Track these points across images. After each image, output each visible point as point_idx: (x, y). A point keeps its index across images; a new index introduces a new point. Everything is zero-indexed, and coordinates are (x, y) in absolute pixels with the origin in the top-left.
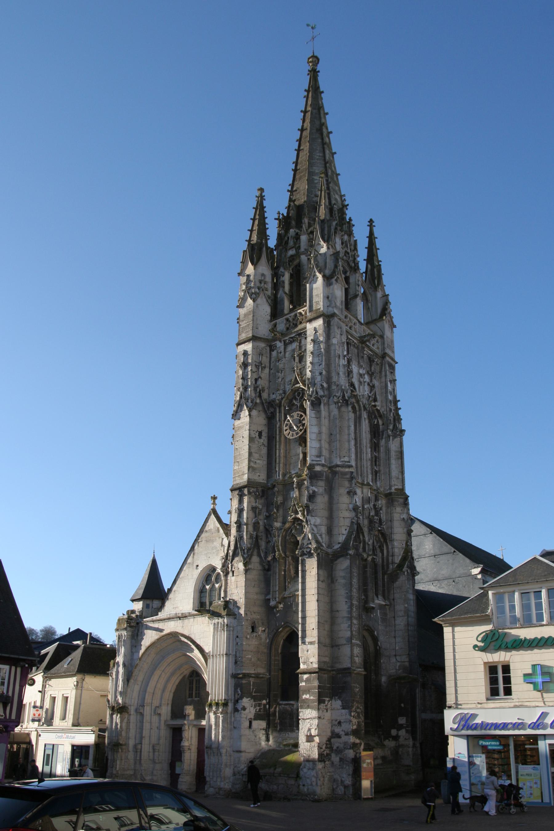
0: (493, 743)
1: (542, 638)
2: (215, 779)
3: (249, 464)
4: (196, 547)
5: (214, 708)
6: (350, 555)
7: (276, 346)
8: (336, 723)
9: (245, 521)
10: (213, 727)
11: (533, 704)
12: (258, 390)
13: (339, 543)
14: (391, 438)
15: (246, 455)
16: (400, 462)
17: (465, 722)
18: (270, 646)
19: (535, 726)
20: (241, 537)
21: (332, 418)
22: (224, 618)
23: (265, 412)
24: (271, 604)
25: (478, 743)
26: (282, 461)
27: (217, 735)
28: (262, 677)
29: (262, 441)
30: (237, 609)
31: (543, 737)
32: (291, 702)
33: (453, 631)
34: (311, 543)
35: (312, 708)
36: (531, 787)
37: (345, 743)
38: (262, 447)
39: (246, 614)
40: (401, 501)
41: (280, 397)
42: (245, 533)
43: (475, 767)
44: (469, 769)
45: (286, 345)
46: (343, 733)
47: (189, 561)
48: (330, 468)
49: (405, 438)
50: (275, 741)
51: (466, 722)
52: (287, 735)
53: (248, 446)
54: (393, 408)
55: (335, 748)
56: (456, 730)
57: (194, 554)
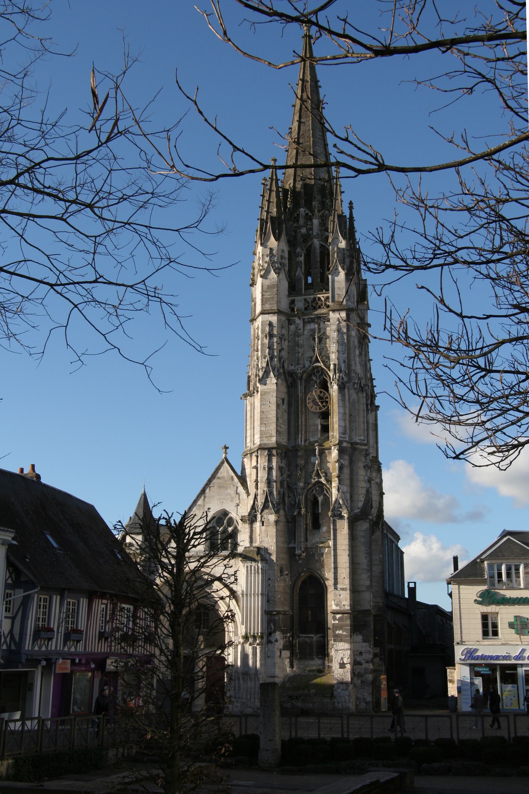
0: (485, 669)
1: (522, 598)
2: (252, 700)
3: (277, 428)
4: (207, 491)
5: (251, 640)
6: (369, 519)
7: (295, 322)
8: (358, 653)
9: (274, 478)
10: (251, 656)
11: (514, 643)
12: (282, 361)
13: (359, 508)
14: (370, 412)
15: (274, 419)
16: (375, 434)
17: (470, 654)
18: (293, 587)
19: (517, 658)
20: (271, 493)
21: (351, 401)
22: (258, 562)
23: (286, 381)
24: (296, 553)
25: (474, 669)
26: (303, 430)
27: (255, 662)
28: (288, 614)
29: (284, 407)
30: (268, 555)
31: (520, 666)
32: (311, 635)
33: (459, 588)
34: (341, 507)
35: (345, 641)
36: (511, 699)
37: (366, 669)
38: (285, 413)
39: (277, 560)
40: (376, 467)
41: (301, 371)
42: (275, 490)
43: (475, 686)
44: (471, 687)
45: (305, 323)
46: (364, 661)
47: (200, 502)
48: (352, 444)
49: (379, 412)
50: (298, 668)
51: (471, 654)
52: (307, 662)
53: (275, 412)
54: (370, 385)
55: (356, 673)
56: (463, 660)
57: (205, 497)
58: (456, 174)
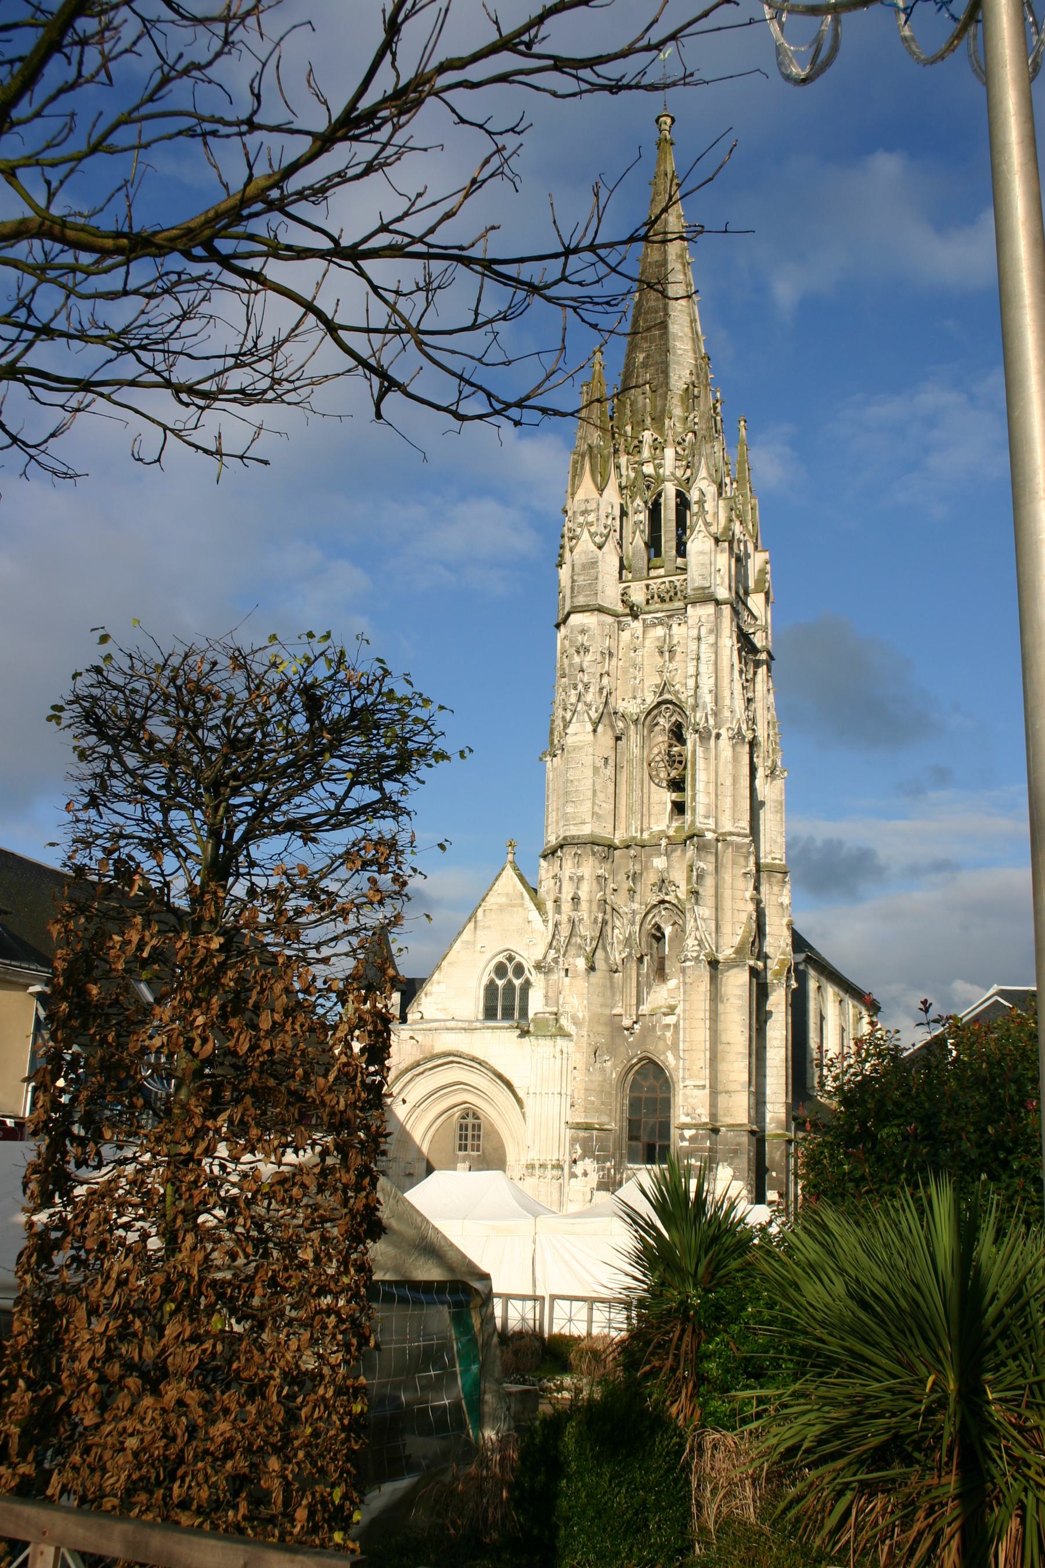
58: (493, 392)
